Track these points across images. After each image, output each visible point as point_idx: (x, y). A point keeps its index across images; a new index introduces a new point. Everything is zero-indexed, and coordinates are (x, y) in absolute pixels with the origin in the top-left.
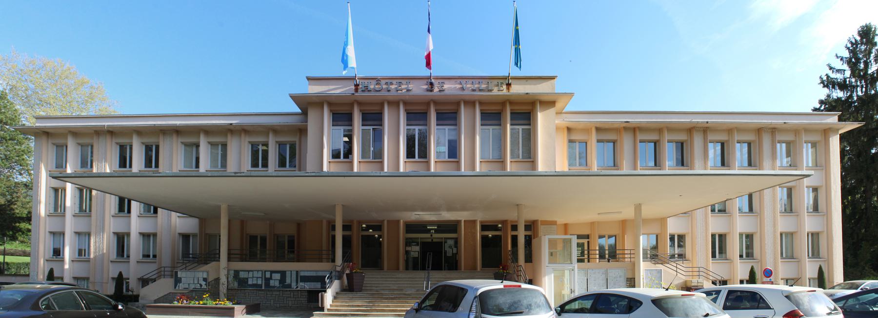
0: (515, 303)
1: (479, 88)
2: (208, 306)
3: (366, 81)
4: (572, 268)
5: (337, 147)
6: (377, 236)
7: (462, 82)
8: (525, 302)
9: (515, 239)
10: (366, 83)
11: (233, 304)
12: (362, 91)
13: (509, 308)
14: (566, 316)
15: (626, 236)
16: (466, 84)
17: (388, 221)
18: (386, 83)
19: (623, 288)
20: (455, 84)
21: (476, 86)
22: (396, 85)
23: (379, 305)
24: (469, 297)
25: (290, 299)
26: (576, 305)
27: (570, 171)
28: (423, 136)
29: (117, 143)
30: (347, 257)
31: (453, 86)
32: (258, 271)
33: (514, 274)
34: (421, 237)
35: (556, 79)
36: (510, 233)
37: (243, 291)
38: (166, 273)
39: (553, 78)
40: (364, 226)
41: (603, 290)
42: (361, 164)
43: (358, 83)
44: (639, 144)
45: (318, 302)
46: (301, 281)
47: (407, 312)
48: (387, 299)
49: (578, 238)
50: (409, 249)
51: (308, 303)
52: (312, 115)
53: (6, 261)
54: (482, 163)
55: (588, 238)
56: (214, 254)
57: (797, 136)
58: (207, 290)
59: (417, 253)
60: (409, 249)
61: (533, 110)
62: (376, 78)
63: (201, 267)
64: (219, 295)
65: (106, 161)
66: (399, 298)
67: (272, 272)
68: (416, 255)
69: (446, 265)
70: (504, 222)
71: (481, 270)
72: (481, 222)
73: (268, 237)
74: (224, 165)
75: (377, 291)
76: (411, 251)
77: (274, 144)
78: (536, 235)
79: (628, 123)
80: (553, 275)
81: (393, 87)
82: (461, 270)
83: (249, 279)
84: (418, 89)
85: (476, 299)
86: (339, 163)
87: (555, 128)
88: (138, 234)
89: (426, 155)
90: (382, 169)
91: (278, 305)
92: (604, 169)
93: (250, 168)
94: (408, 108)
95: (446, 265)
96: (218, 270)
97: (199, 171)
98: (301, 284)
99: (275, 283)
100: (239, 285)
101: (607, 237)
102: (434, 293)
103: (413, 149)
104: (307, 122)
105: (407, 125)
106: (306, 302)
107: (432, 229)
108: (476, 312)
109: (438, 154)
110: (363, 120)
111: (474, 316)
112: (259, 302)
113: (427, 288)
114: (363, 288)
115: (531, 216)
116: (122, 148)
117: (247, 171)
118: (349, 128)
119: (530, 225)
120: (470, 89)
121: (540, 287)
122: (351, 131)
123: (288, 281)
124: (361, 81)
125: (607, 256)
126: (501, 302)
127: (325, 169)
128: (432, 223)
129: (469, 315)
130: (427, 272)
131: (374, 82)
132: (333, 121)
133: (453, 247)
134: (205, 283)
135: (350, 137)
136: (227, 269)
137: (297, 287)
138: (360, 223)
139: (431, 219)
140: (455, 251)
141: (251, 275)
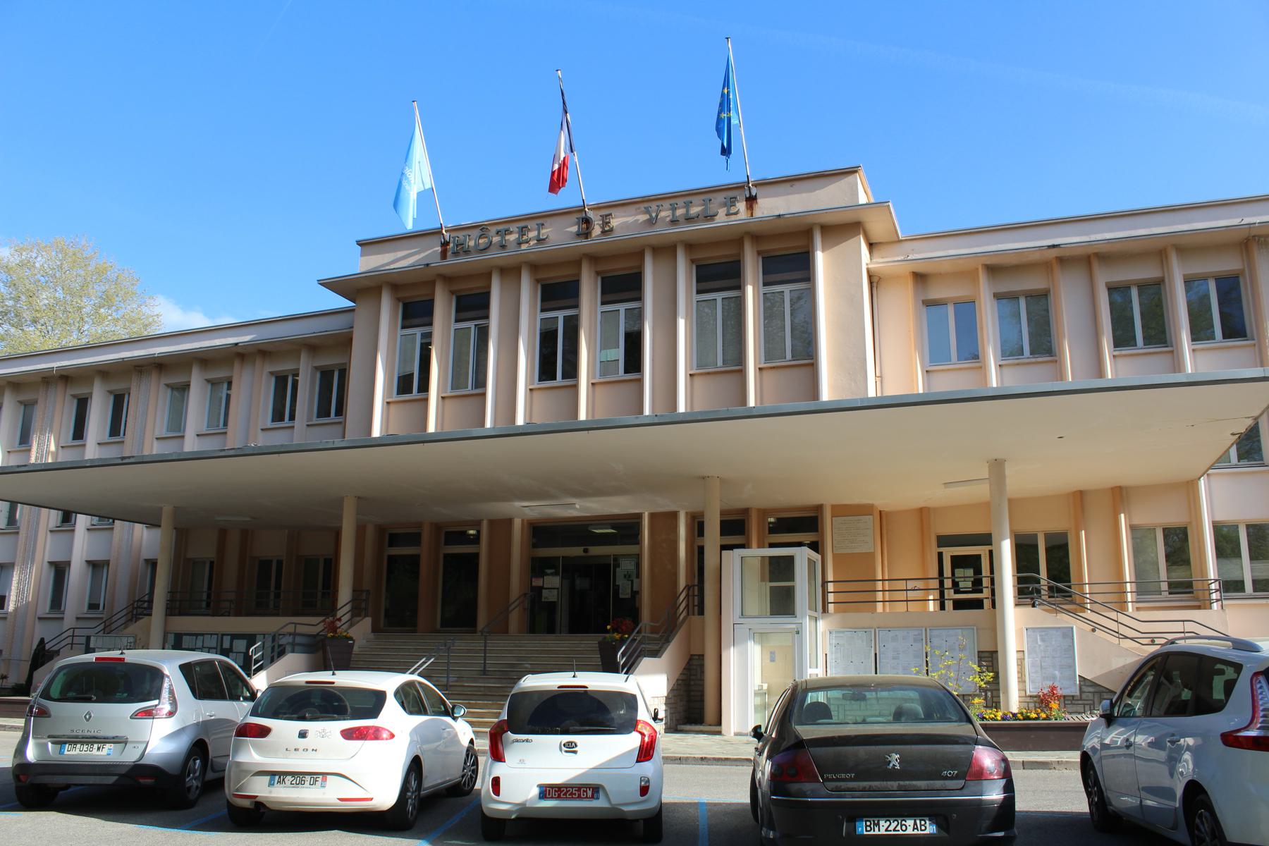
3: (461, 234)
5: (408, 372)
20: (636, 215)
29: (74, 396)
31: (630, 219)
32: (211, 634)
38: (76, 640)
50: (537, 582)
53: (297, 631)
57: (1165, 263)
59: (555, 592)
65: (51, 432)
73: (284, 562)
77: (309, 371)
81: (512, 238)
84: (560, 236)
86: (774, 371)
88: (84, 564)
116: (281, 381)
120: (668, 219)
131: (477, 233)
132: (764, 274)
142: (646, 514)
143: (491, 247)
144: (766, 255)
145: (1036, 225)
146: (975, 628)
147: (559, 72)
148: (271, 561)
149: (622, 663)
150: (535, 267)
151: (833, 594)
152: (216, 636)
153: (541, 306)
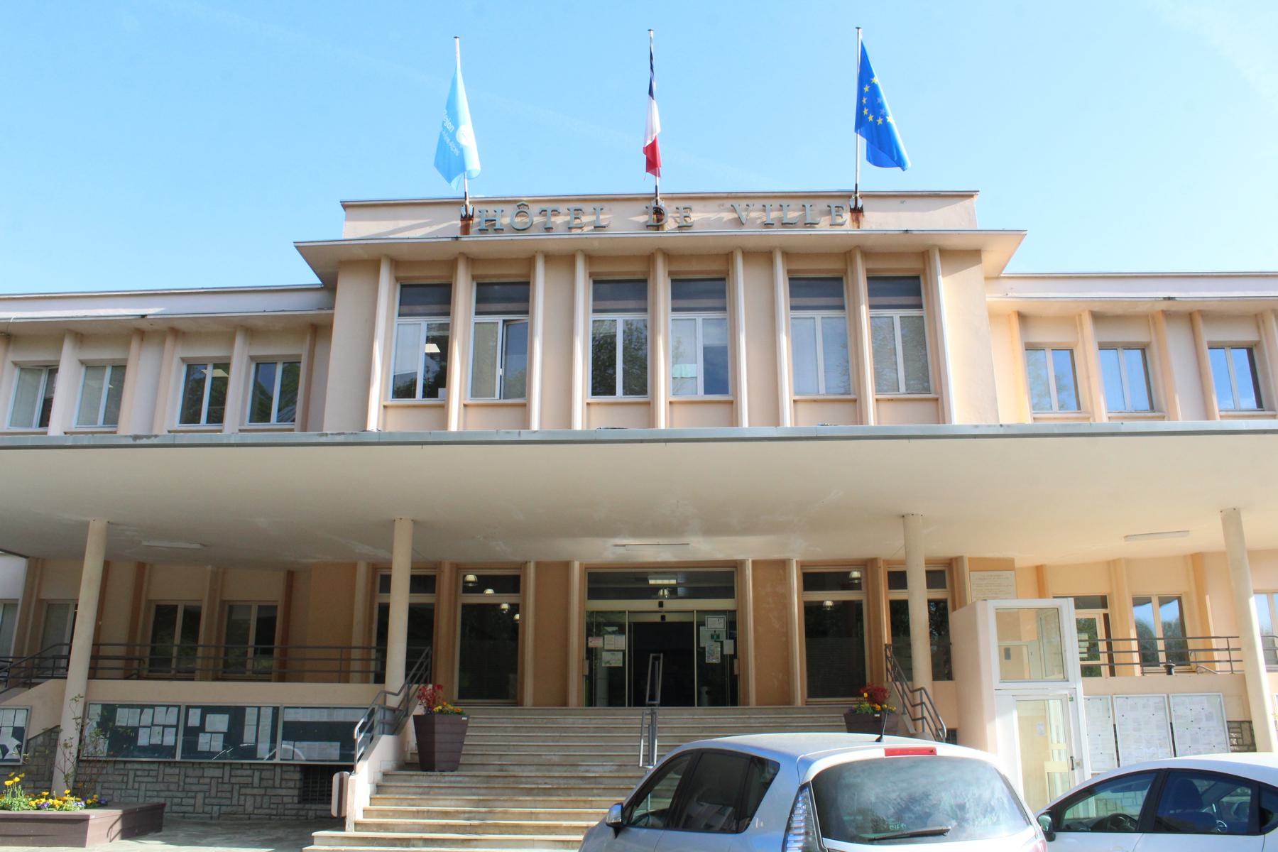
0: (913, 800)
1: (780, 219)
2: (14, 812)
3: (491, 208)
4: (1066, 692)
5: (406, 369)
6: (505, 606)
7: (736, 206)
8: (946, 799)
9: (900, 611)
10: (491, 212)
11: (87, 806)
12: (480, 230)
13: (899, 817)
14: (1069, 840)
15: (1207, 597)
16: (746, 210)
17: (538, 564)
18: (543, 212)
19: (1221, 752)
21: (774, 215)
22: (568, 215)
23: (505, 813)
24: (783, 788)
25: (248, 791)
26: (1089, 809)
27: (1039, 423)
28: (638, 337)
30: (418, 669)
31: (713, 216)
32: (168, 707)
33: (904, 713)
34: (632, 609)
35: (975, 199)
36: (886, 596)
37: (122, 766)
39: (968, 195)
40: (471, 578)
41: (1161, 759)
42: (470, 411)
43: (470, 212)
44: (1209, 355)
45: (329, 802)
46: (284, 738)
47: (590, 832)
48: (529, 792)
49: (1077, 607)
50: (595, 642)
51: (299, 803)
52: (348, 291)
54: (800, 406)
55: (1105, 606)
56: (54, 658)
58: (20, 763)
60: (595, 642)
61: (924, 271)
62: (515, 202)
63: (15, 695)
64: (50, 780)
66: (567, 791)
67: (207, 710)
68: (616, 660)
69: (705, 689)
70: (868, 565)
71: (807, 703)
72: (802, 565)
74: (112, 418)
75: (502, 767)
76: (603, 649)
78: (960, 600)
79: (1170, 302)
80: (1015, 715)
81: (559, 220)
82: (746, 703)
83: (141, 731)
85: (807, 793)
87: (987, 314)
89: (646, 385)
90: (526, 423)
91: (216, 808)
92: (1125, 418)
93: (176, 425)
94: (597, 269)
95: (705, 689)
96: (58, 705)
97: (46, 433)
98: (285, 746)
99: (211, 742)
100: (110, 747)
101: (1155, 601)
102: (669, 775)
103: (594, 373)
104: (332, 308)
105: (595, 311)
106: (296, 800)
107: (663, 587)
108: (807, 833)
109: (678, 383)
110: (479, 301)
111: (800, 845)
112: (162, 801)
113: (649, 759)
114: (462, 760)
115: (943, 548)
117: (169, 432)
118: (442, 320)
119: (942, 572)
120: (759, 221)
121: (981, 749)
122: (446, 327)
123: (248, 737)
124: (478, 208)
125: (1162, 657)
126: (873, 799)
127: (373, 424)
128: (663, 569)
129: (785, 842)
130: (647, 710)
131: (511, 209)
132: (400, 304)
133: (723, 636)
134: (17, 742)
135: (443, 343)
136: (82, 701)
137: (273, 757)
138: (460, 569)
139: (660, 559)
140: (728, 650)
141: (147, 717)
142: (750, 561)
143: (531, 228)
144: (481, 281)
145: (9, 299)
146: (1221, 694)
147: (652, 32)
148: (176, 607)
149: (359, 741)
150: (590, 258)
151: (1134, 662)
152: (176, 709)
153: (593, 305)
